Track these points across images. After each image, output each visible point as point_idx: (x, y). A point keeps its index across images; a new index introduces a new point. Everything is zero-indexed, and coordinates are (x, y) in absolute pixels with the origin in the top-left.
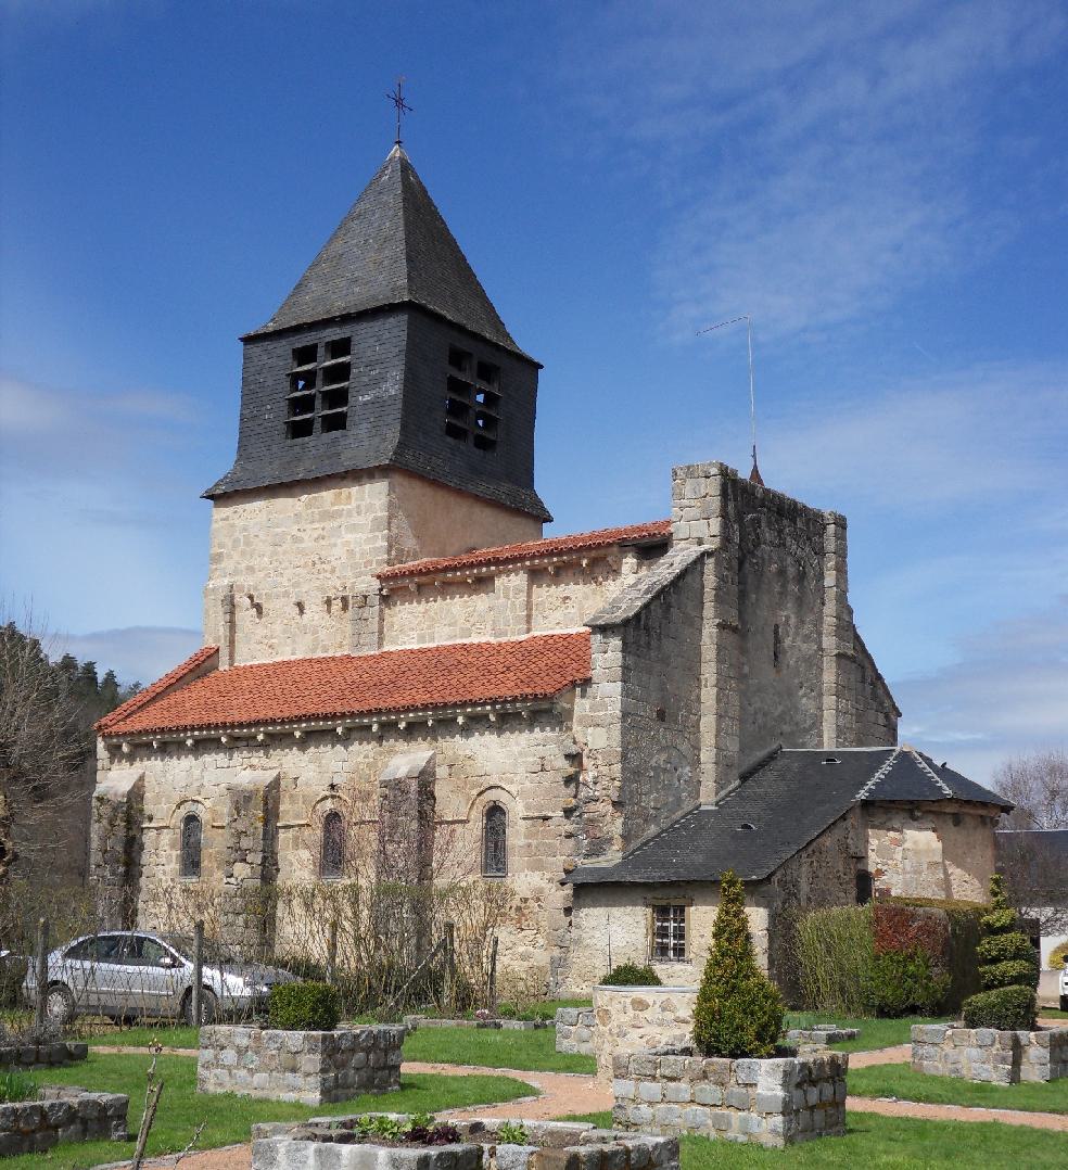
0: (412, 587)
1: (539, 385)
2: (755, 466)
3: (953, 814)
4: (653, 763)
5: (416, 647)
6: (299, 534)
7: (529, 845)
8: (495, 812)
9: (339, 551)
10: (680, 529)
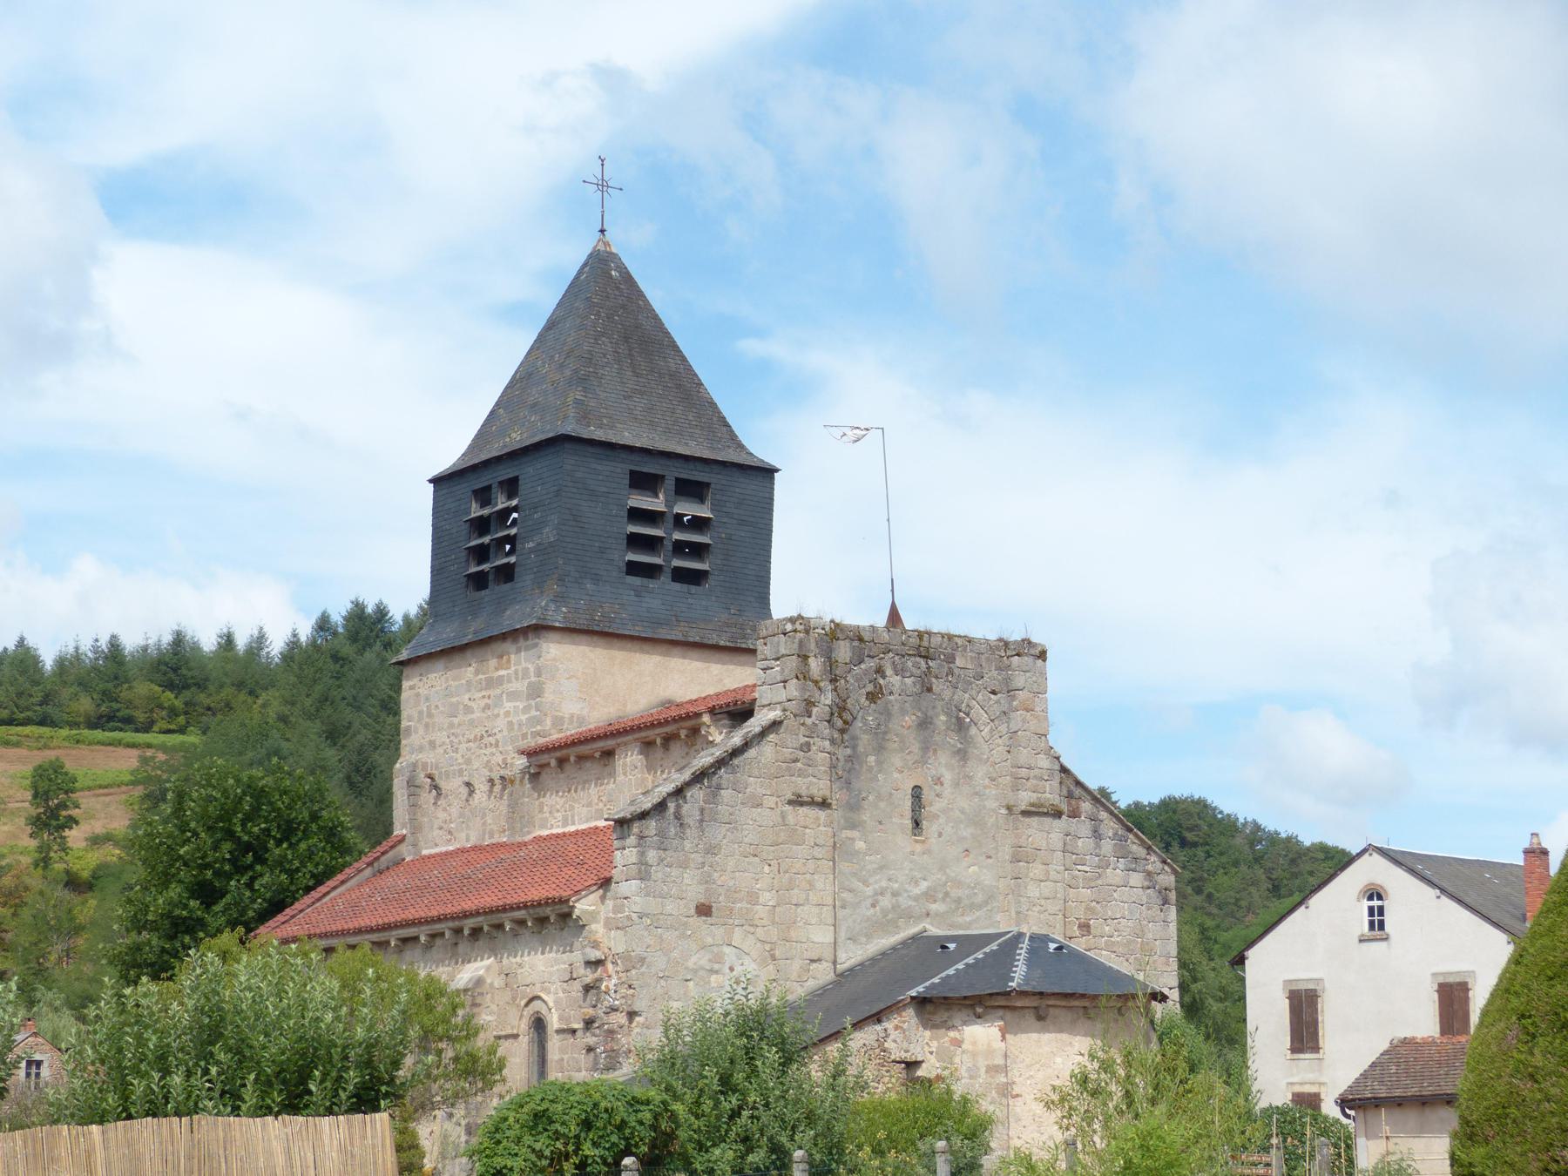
0: (553, 763)
1: (775, 503)
2: (893, 603)
3: (1035, 1008)
4: (690, 964)
5: (560, 831)
6: (470, 704)
7: (562, 1060)
8: (539, 1024)
9: (501, 723)
10: (764, 695)
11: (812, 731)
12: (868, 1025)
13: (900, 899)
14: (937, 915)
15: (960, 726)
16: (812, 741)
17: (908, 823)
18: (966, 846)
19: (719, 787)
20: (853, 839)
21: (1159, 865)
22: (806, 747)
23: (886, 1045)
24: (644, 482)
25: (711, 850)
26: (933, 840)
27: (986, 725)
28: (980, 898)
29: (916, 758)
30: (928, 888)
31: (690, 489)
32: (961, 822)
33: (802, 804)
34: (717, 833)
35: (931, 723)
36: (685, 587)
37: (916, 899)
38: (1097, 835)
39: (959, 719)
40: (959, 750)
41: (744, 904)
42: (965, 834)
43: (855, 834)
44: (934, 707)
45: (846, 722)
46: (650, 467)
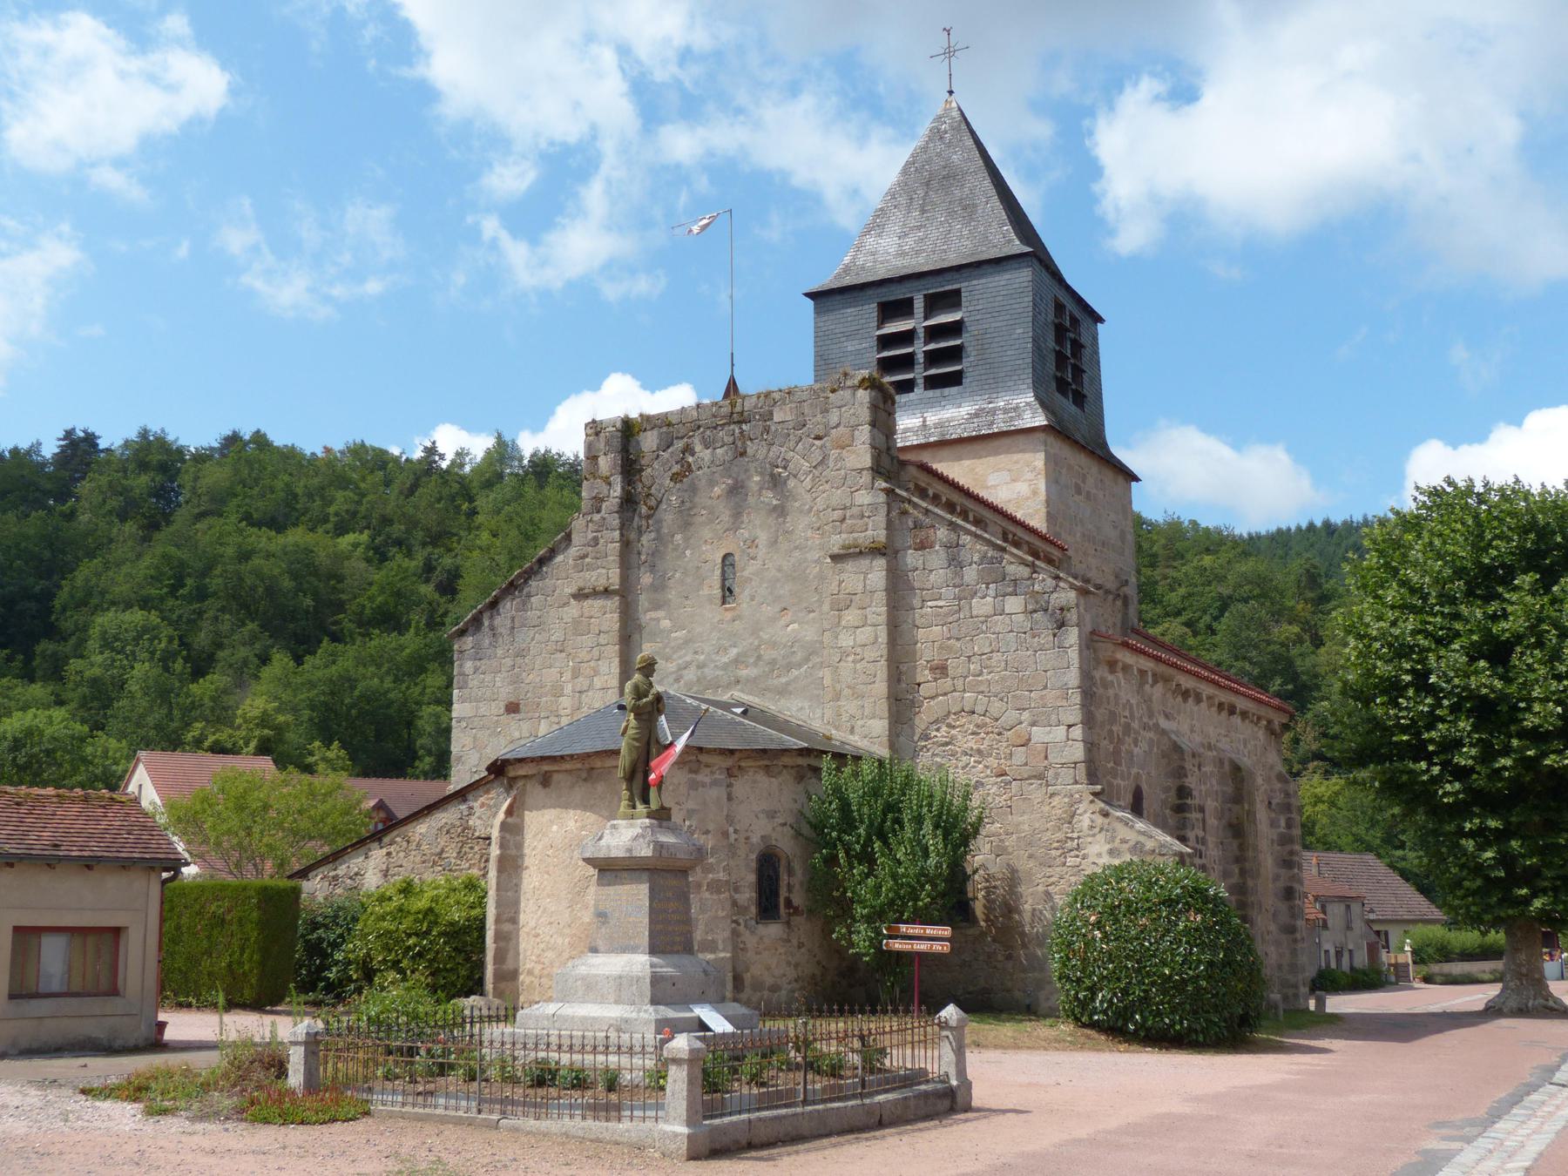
11: (602, 525)
12: (456, 802)
13: (706, 670)
14: (748, 681)
15: (776, 482)
16: (599, 534)
17: (717, 592)
18: (783, 605)
19: (529, 596)
20: (658, 620)
21: (1050, 582)
22: (596, 541)
23: (471, 823)
24: (891, 310)
25: (521, 654)
26: (745, 605)
27: (807, 474)
28: (799, 656)
29: (726, 526)
30: (738, 655)
31: (935, 303)
32: (778, 580)
33: (587, 596)
34: (523, 636)
35: (742, 487)
36: (938, 392)
37: (725, 667)
38: (955, 563)
39: (772, 475)
40: (775, 508)
41: (549, 698)
42: (782, 592)
43: (660, 614)
44: (747, 471)
45: (650, 508)
46: (898, 293)
